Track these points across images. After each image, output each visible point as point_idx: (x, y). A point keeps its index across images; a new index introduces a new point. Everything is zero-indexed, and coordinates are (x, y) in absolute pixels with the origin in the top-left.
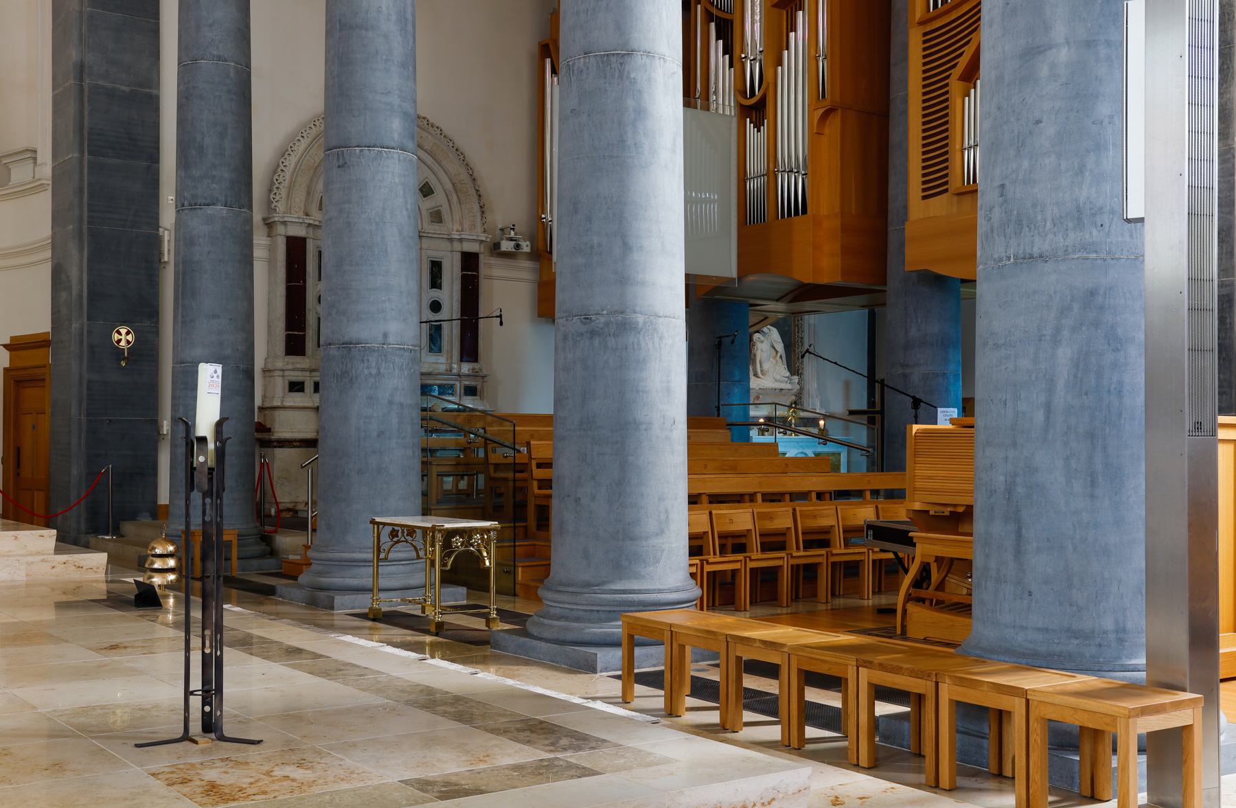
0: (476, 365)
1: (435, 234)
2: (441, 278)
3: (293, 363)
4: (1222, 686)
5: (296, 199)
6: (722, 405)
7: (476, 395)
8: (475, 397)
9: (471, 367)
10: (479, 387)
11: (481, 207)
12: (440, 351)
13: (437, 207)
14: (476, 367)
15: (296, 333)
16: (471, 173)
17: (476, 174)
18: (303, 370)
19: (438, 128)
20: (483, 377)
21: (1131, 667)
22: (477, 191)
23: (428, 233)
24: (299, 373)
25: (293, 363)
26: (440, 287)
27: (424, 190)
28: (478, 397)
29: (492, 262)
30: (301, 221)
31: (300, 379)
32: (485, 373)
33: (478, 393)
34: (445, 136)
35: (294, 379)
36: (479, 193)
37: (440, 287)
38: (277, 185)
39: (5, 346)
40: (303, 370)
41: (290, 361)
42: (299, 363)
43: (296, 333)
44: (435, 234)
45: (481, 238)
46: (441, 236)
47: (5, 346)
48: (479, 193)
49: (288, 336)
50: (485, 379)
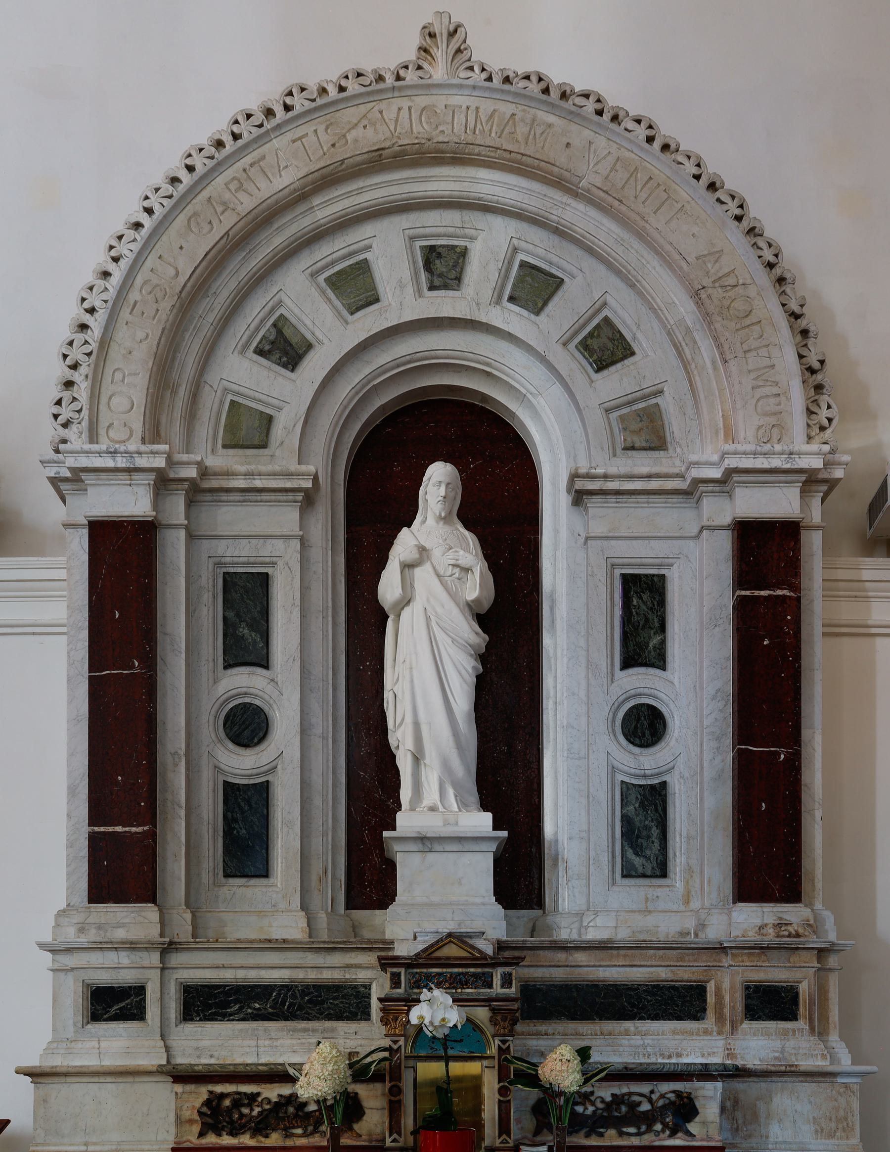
0: (793, 913)
1: (631, 477)
2: (662, 628)
4: (65, 621)
5: (115, 401)
7: (794, 1017)
8: (789, 1025)
9: (770, 920)
10: (804, 988)
11: (812, 371)
12: (662, 870)
13: (645, 398)
14: (788, 917)
15: (119, 829)
16: (769, 256)
17: (786, 265)
18: (132, 946)
19: (639, 121)
20: (822, 953)
22: (796, 316)
23: (605, 477)
24: (124, 958)
25: (100, 927)
26: (659, 660)
27: (594, 343)
28: (801, 1024)
29: (866, 575)
30: (121, 462)
31: (127, 977)
32: (832, 937)
33: (802, 1010)
34: (665, 147)
35: (104, 978)
36: (803, 323)
37: (659, 660)
38: (77, 377)
39: (42, 946)
40: (132, 946)
41: (91, 920)
42: (122, 925)
43: (119, 829)
44: (631, 477)
45: (804, 463)
46: (654, 485)
47: (42, 946)
48: (803, 323)
49: (93, 839)
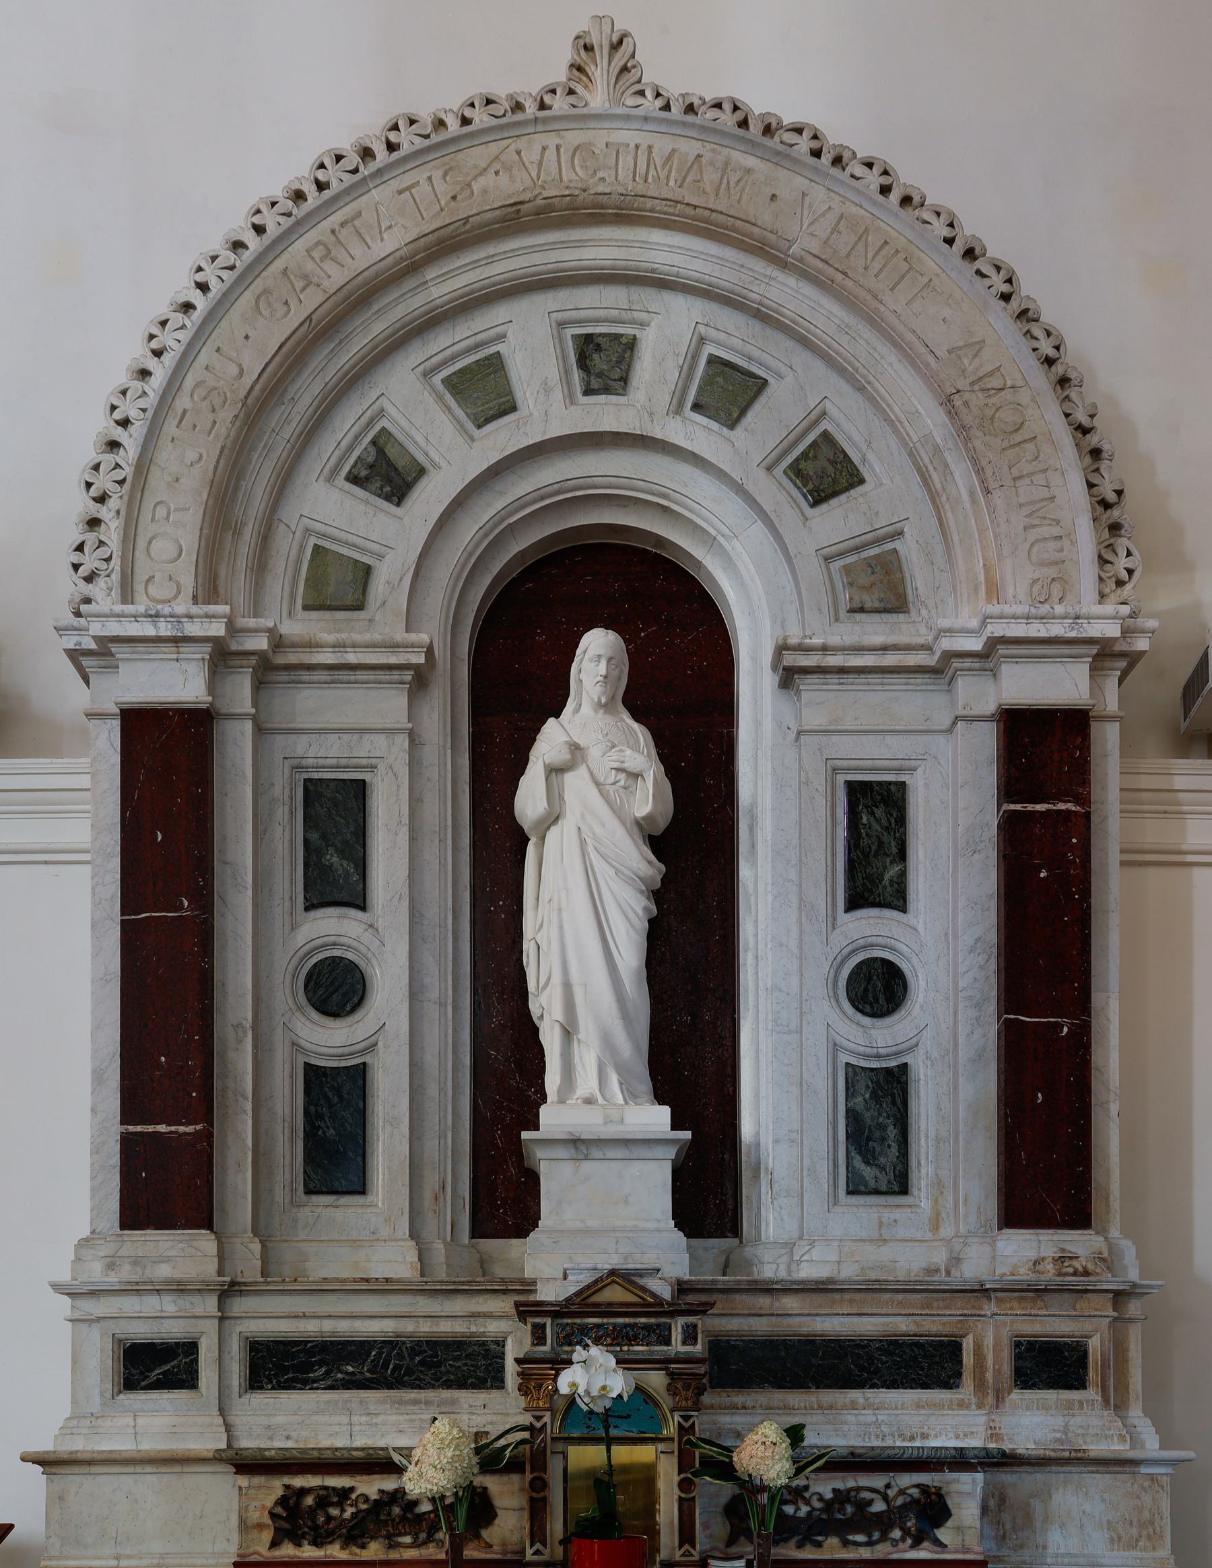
0: (1080, 1243)
1: (859, 649)
2: (902, 855)
3: (136, 1262)
5: (157, 545)
6: (673, 1439)
7: (1081, 1384)
8: (1074, 1395)
9: (1049, 1252)
10: (1094, 1345)
12: (901, 1185)
13: (878, 541)
14: (1073, 1249)
15: (162, 1128)
16: (1047, 349)
17: (1070, 361)
18: (180, 1288)
20: (1119, 1297)
21: (223, 571)
23: (824, 649)
24: (169, 1304)
25: (136, 1262)
26: (897, 899)
27: (809, 467)
28: (1091, 1394)
29: (1179, 782)
31: (173, 1330)
32: (1133, 1275)
33: (1093, 1374)
34: (906, 201)
35: (142, 1331)
36: (1093, 440)
37: (897, 899)
38: (104, 513)
39: (57, 1287)
40: (180, 1288)
41: (124, 1252)
42: (167, 1260)
43: (162, 1128)
44: (859, 649)
46: (890, 660)
47: (57, 1287)
48: (1093, 440)
49: (127, 1142)
50: (1134, 1308)
